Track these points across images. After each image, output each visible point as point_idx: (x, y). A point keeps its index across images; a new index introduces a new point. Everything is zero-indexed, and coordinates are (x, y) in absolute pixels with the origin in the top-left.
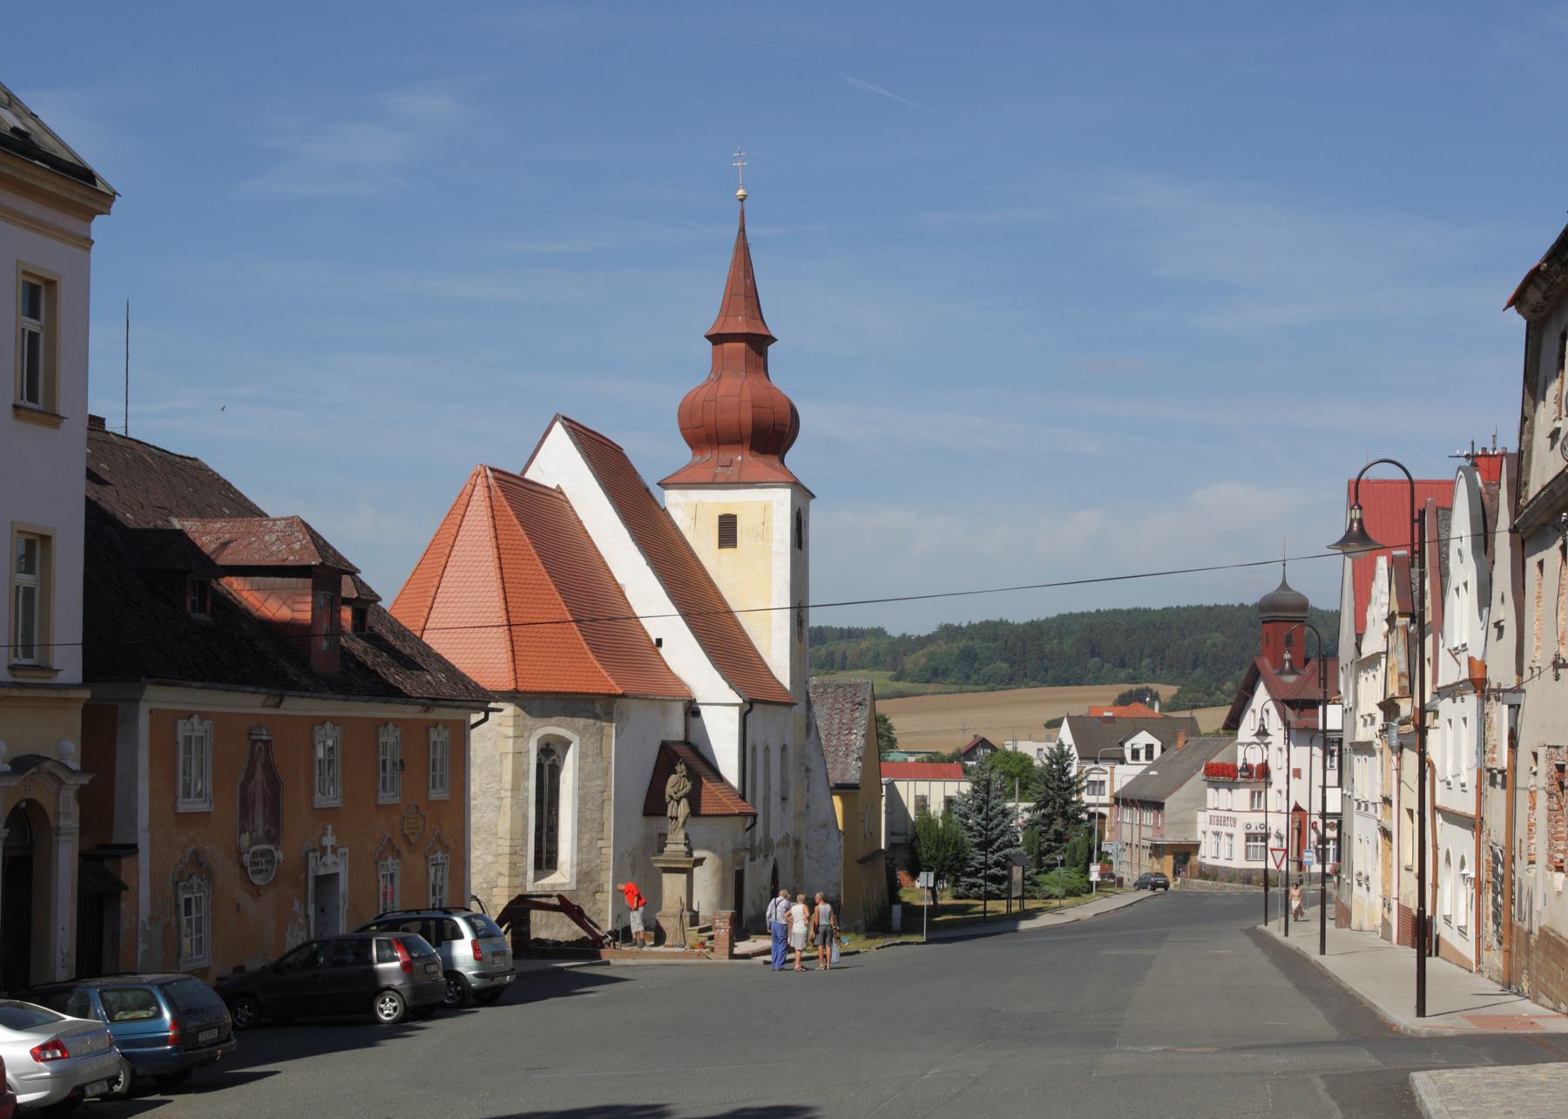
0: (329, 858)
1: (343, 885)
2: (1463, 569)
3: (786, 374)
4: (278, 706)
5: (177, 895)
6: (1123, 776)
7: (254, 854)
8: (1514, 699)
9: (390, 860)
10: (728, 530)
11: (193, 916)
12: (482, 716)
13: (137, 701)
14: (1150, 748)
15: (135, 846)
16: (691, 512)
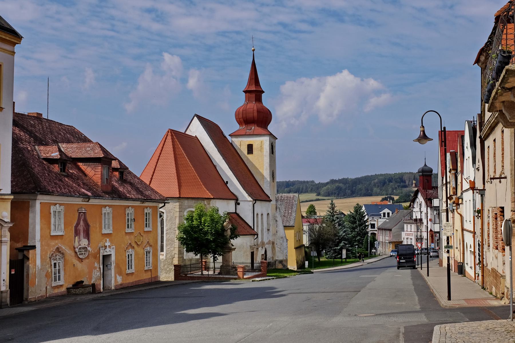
0: (108, 249)
1: (113, 258)
2: (468, 153)
3: (267, 101)
4: (88, 201)
5: (51, 262)
6: (380, 222)
7: (80, 248)
8: (482, 192)
9: (130, 250)
10: (250, 149)
11: (57, 268)
12: (163, 204)
13: (36, 200)
14: (388, 214)
15: (35, 246)
16: (241, 144)
